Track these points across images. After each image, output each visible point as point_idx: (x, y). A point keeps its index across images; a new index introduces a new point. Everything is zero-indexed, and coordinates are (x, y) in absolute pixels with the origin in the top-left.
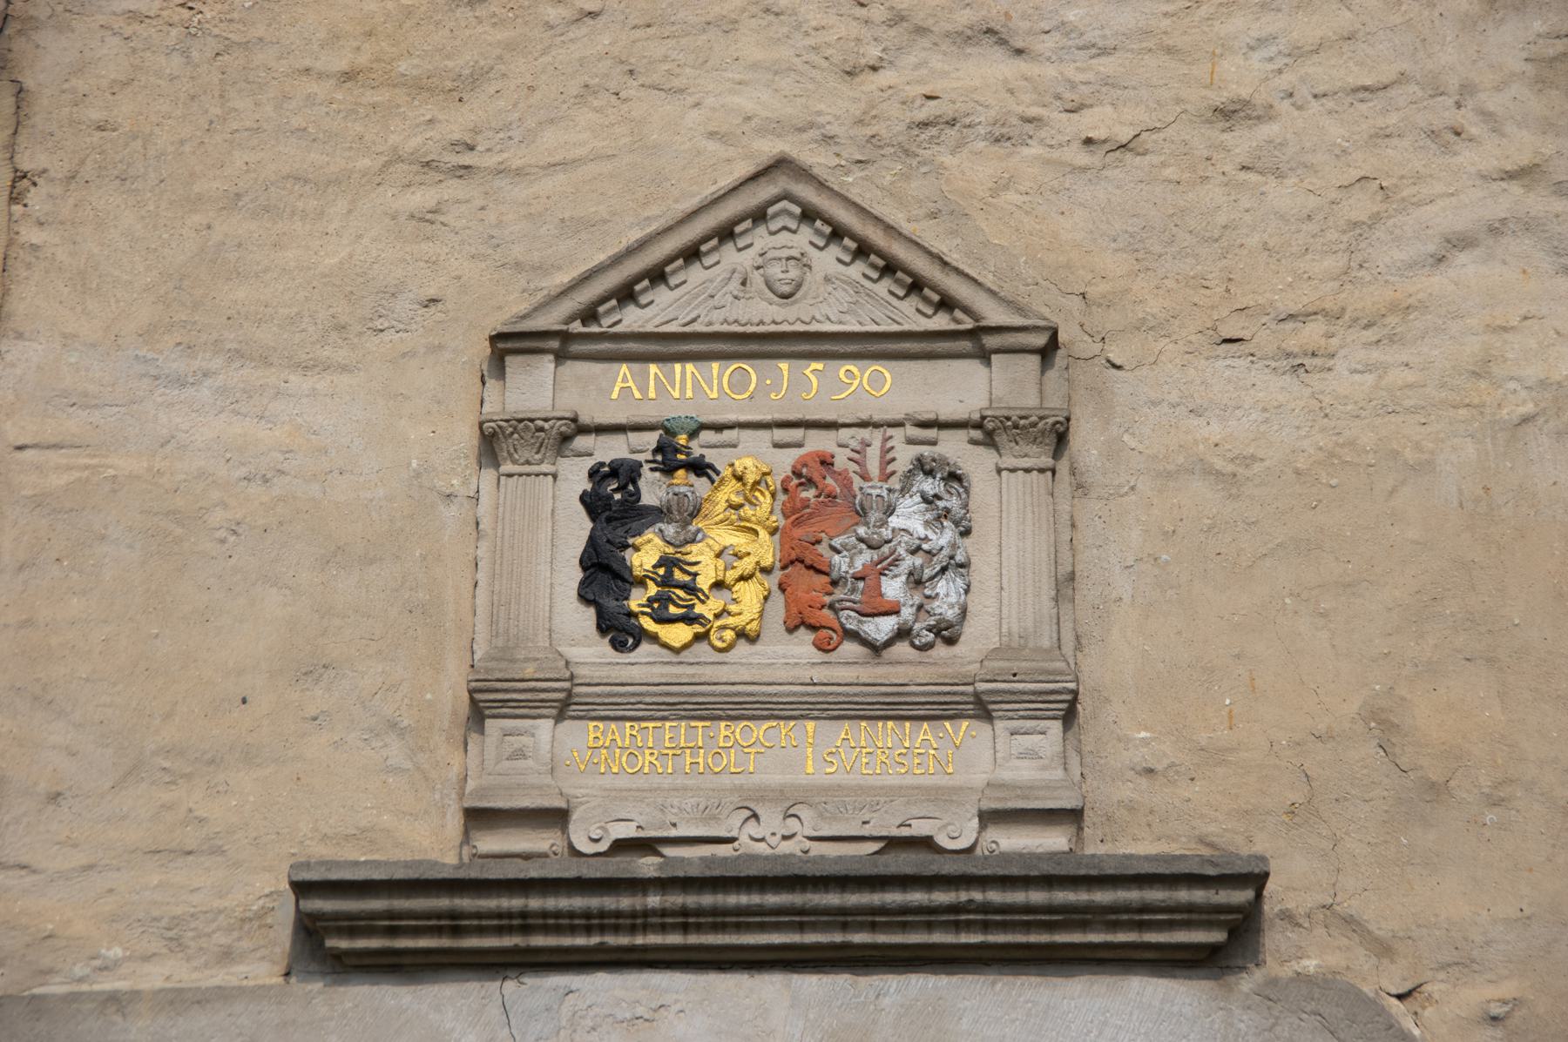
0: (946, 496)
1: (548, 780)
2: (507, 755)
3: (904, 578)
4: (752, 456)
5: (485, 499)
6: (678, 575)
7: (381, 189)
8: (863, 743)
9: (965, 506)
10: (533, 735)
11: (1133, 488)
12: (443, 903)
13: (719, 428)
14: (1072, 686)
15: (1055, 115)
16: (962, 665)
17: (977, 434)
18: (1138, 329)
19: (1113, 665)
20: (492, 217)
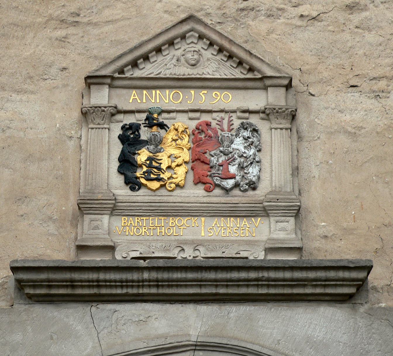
0: (253, 137)
1: (107, 236)
2: (92, 228)
3: (237, 166)
4: (181, 122)
5: (83, 138)
6: (154, 164)
7: (45, 30)
8: (222, 226)
9: (259, 141)
10: (101, 221)
11: (319, 138)
12: (67, 276)
13: (169, 112)
14: (298, 204)
15: (289, 8)
16: (259, 197)
17: (262, 115)
18: (320, 82)
19: (314, 198)
20: (86, 40)
